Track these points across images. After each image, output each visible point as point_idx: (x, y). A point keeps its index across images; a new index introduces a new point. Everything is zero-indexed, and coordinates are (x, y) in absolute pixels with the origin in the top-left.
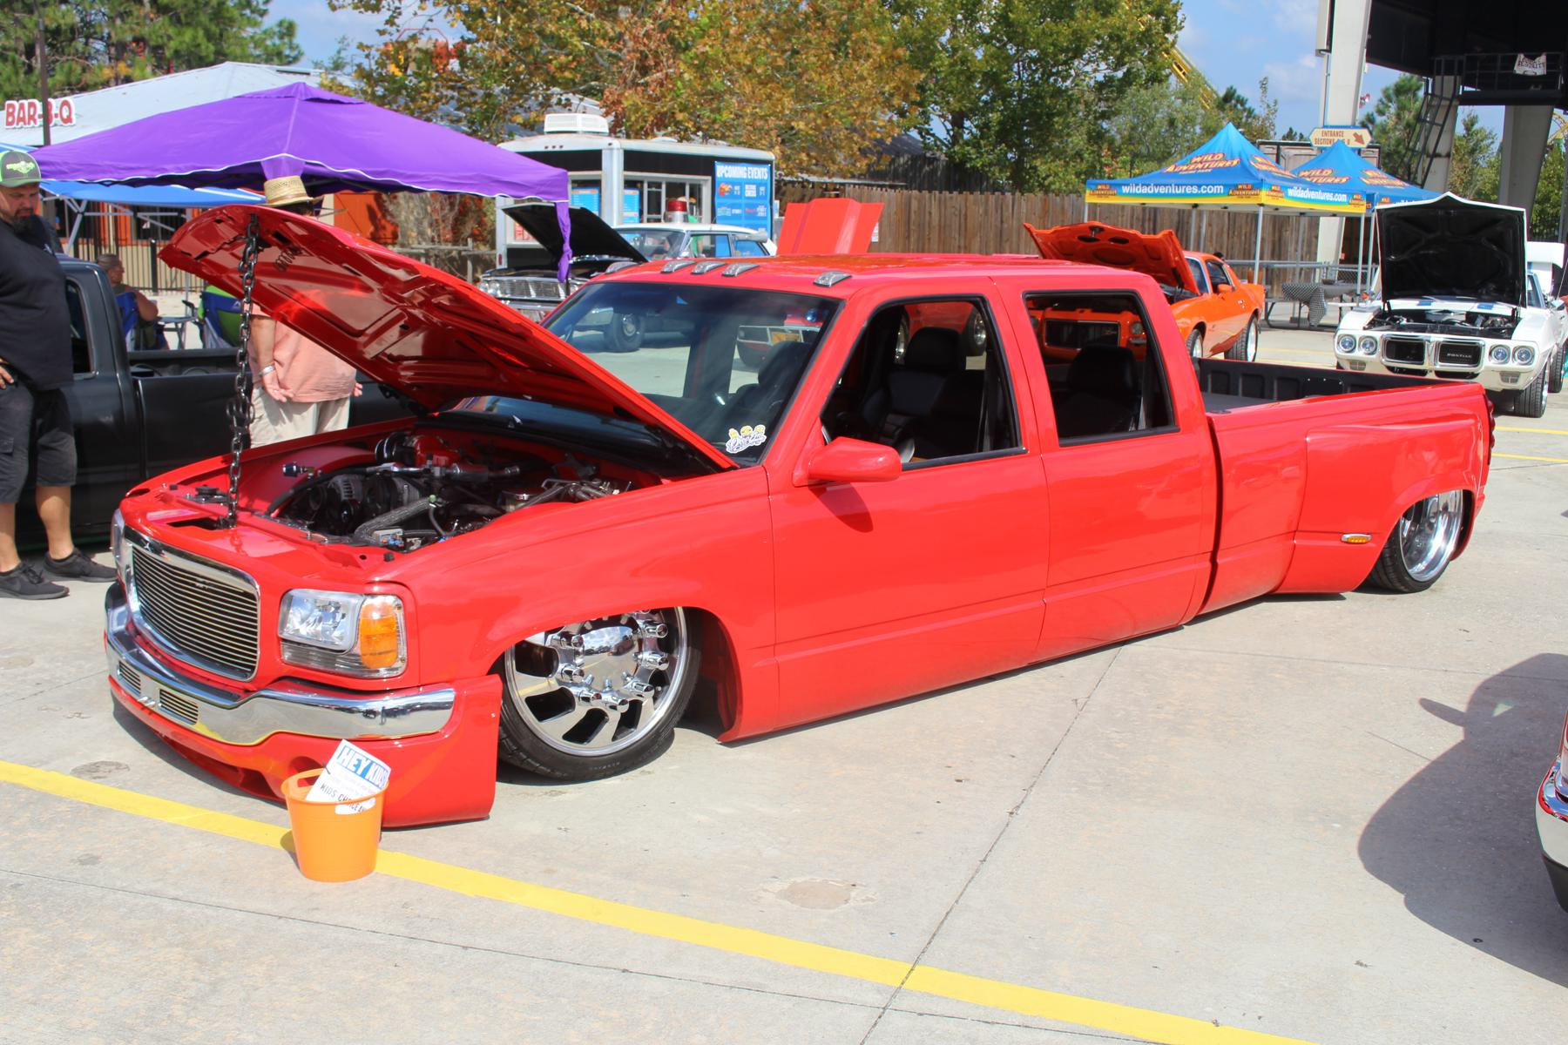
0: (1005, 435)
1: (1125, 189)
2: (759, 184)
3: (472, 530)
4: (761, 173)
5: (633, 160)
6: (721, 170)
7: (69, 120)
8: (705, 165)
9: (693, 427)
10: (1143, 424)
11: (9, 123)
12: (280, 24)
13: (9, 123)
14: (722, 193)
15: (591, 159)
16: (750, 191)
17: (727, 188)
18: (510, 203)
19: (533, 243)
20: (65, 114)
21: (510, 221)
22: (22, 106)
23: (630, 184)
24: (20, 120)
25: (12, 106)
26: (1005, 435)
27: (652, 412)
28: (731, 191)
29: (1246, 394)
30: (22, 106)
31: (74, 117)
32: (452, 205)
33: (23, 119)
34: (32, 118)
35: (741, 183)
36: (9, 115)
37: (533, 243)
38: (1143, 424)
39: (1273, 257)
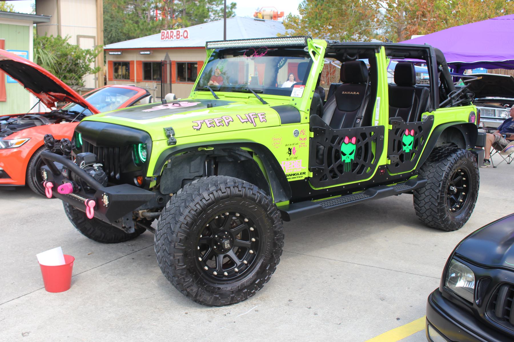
0: (137, 61)
3: (69, 218)
7: (187, 37)
10: (508, 298)
11: (162, 39)
12: (232, 4)
13: (162, 39)
20: (185, 36)
22: (168, 33)
24: (167, 37)
25: (164, 32)
26: (137, 61)
30: (168, 33)
31: (189, 36)
32: (502, 145)
33: (168, 37)
34: (171, 37)
36: (162, 35)
38: (508, 298)
39: (299, 121)
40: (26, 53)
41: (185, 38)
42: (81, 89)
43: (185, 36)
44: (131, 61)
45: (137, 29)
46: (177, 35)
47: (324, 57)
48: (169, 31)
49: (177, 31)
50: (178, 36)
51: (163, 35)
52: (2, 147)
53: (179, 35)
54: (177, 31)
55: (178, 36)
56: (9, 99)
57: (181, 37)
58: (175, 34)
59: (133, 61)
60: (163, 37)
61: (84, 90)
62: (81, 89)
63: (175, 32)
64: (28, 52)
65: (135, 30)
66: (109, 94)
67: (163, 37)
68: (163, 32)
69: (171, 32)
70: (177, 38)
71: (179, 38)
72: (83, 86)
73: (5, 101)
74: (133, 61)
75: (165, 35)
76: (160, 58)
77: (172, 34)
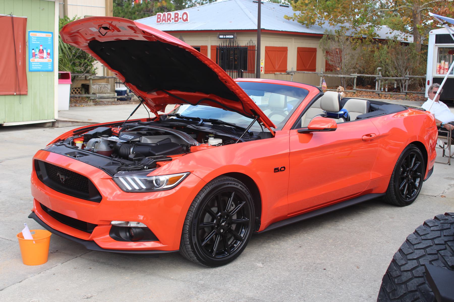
0: (212, 47)
7: (186, 20)
11: (158, 22)
13: (158, 22)
22: (164, 15)
24: (163, 20)
25: (160, 15)
26: (212, 47)
30: (164, 15)
31: (188, 19)
33: (165, 20)
34: (169, 19)
36: (158, 18)
40: (51, 34)
41: (184, 21)
42: (92, 77)
43: (184, 19)
44: (202, 46)
45: (120, 12)
46: (175, 17)
47: (436, 43)
48: (166, 14)
49: (175, 14)
50: (176, 19)
51: (160, 18)
52: (127, 189)
53: (177, 17)
54: (175, 14)
55: (176, 19)
56: (30, 91)
57: (179, 20)
58: (173, 16)
59: (206, 47)
60: (159, 20)
61: (96, 78)
62: (92, 77)
63: (173, 14)
64: (52, 33)
65: (119, 13)
66: (121, 81)
67: (159, 20)
68: (158, 15)
69: (168, 14)
70: (175, 21)
71: (177, 21)
72: (94, 74)
73: (26, 95)
74: (206, 47)
75: (161, 18)
76: (243, 42)
77: (169, 16)
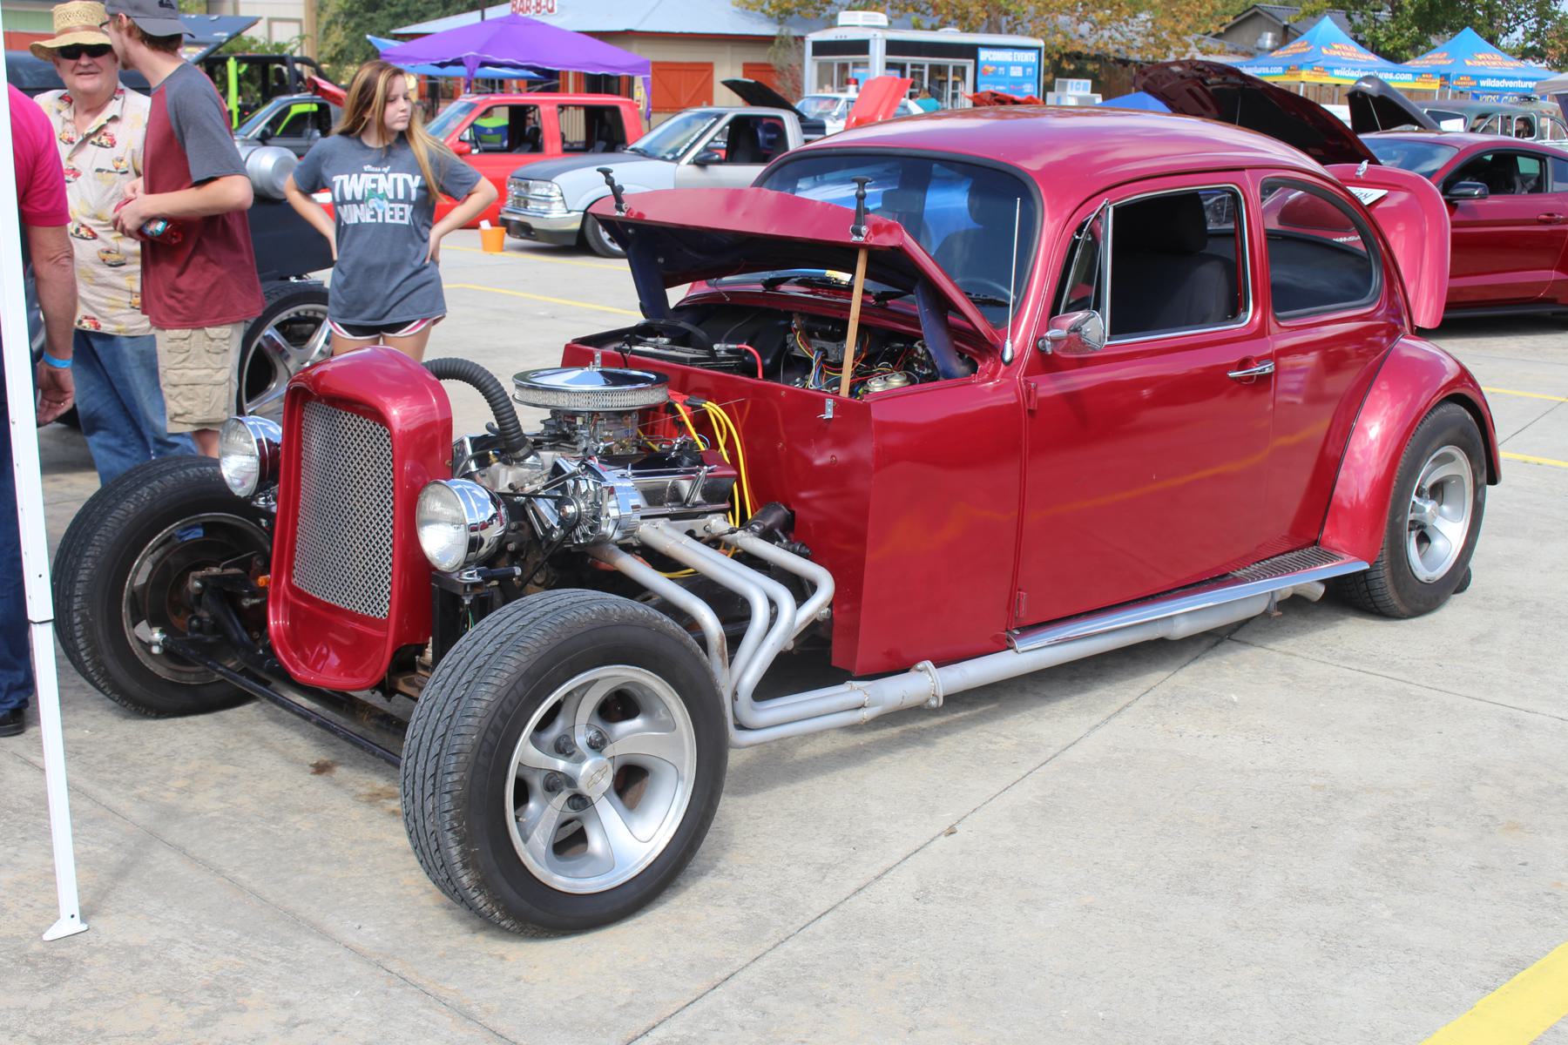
1: (1336, 72)
2: (1025, 66)
4: (1031, 57)
5: (893, 47)
6: (984, 55)
7: (551, 11)
8: (971, 51)
9: (42, 802)
14: (985, 73)
15: (861, 47)
16: (1016, 72)
17: (991, 69)
18: (738, 75)
19: (1349, 125)
21: (726, 90)
23: (889, 66)
27: (575, 886)
28: (995, 73)
29: (1452, 292)
35: (1007, 65)
37: (1349, 125)
